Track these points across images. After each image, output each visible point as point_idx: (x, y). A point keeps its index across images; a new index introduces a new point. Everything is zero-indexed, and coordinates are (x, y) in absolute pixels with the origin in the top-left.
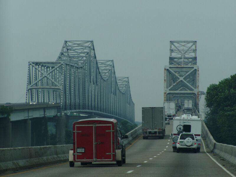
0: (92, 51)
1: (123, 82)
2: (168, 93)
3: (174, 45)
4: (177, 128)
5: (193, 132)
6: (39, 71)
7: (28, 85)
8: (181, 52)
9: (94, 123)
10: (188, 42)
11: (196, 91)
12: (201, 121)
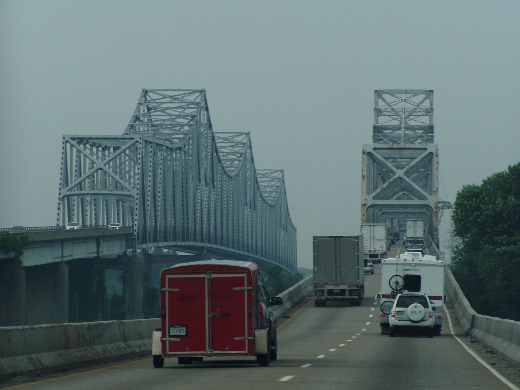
1: (270, 181)
2: (369, 204)
3: (383, 99)
5: (426, 290)
6: (85, 156)
8: (398, 115)
9: (208, 272)
10: (415, 93)
11: (431, 201)
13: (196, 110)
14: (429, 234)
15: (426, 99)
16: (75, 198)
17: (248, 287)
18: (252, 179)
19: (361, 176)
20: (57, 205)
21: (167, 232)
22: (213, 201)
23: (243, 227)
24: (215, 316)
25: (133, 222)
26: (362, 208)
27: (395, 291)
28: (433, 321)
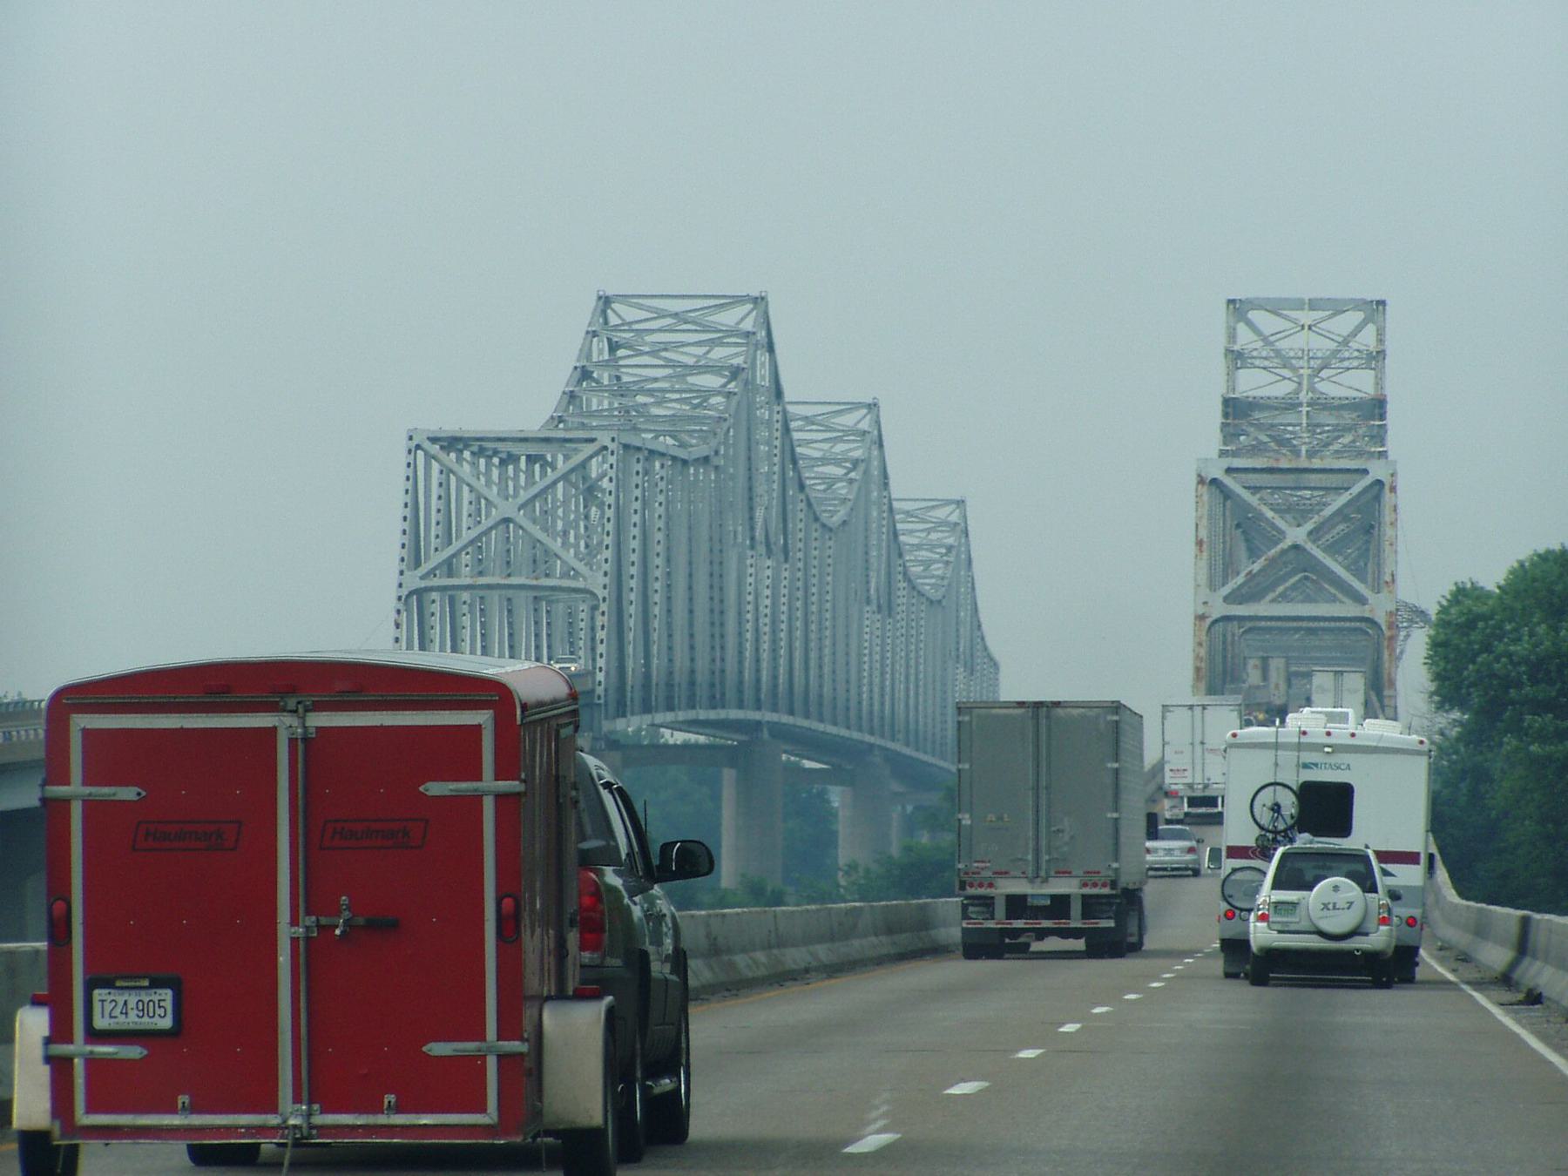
0: (763, 357)
1: (929, 531)
2: (1216, 615)
3: (1250, 324)
4: (1256, 803)
5: (1368, 833)
6: (460, 480)
7: (404, 567)
8: (1294, 369)
9: (291, 703)
10: (1337, 307)
11: (1379, 607)
12: (1418, 753)
13: (744, 349)
14: (1373, 689)
15: (1366, 325)
16: (435, 595)
17: (497, 779)
18: (884, 530)
19: (1193, 544)
20: (393, 615)
21: (672, 685)
22: (784, 596)
23: (860, 663)
24: (326, 930)
25: (594, 660)
26: (1195, 625)
27: (1270, 836)
28: (1391, 936)
